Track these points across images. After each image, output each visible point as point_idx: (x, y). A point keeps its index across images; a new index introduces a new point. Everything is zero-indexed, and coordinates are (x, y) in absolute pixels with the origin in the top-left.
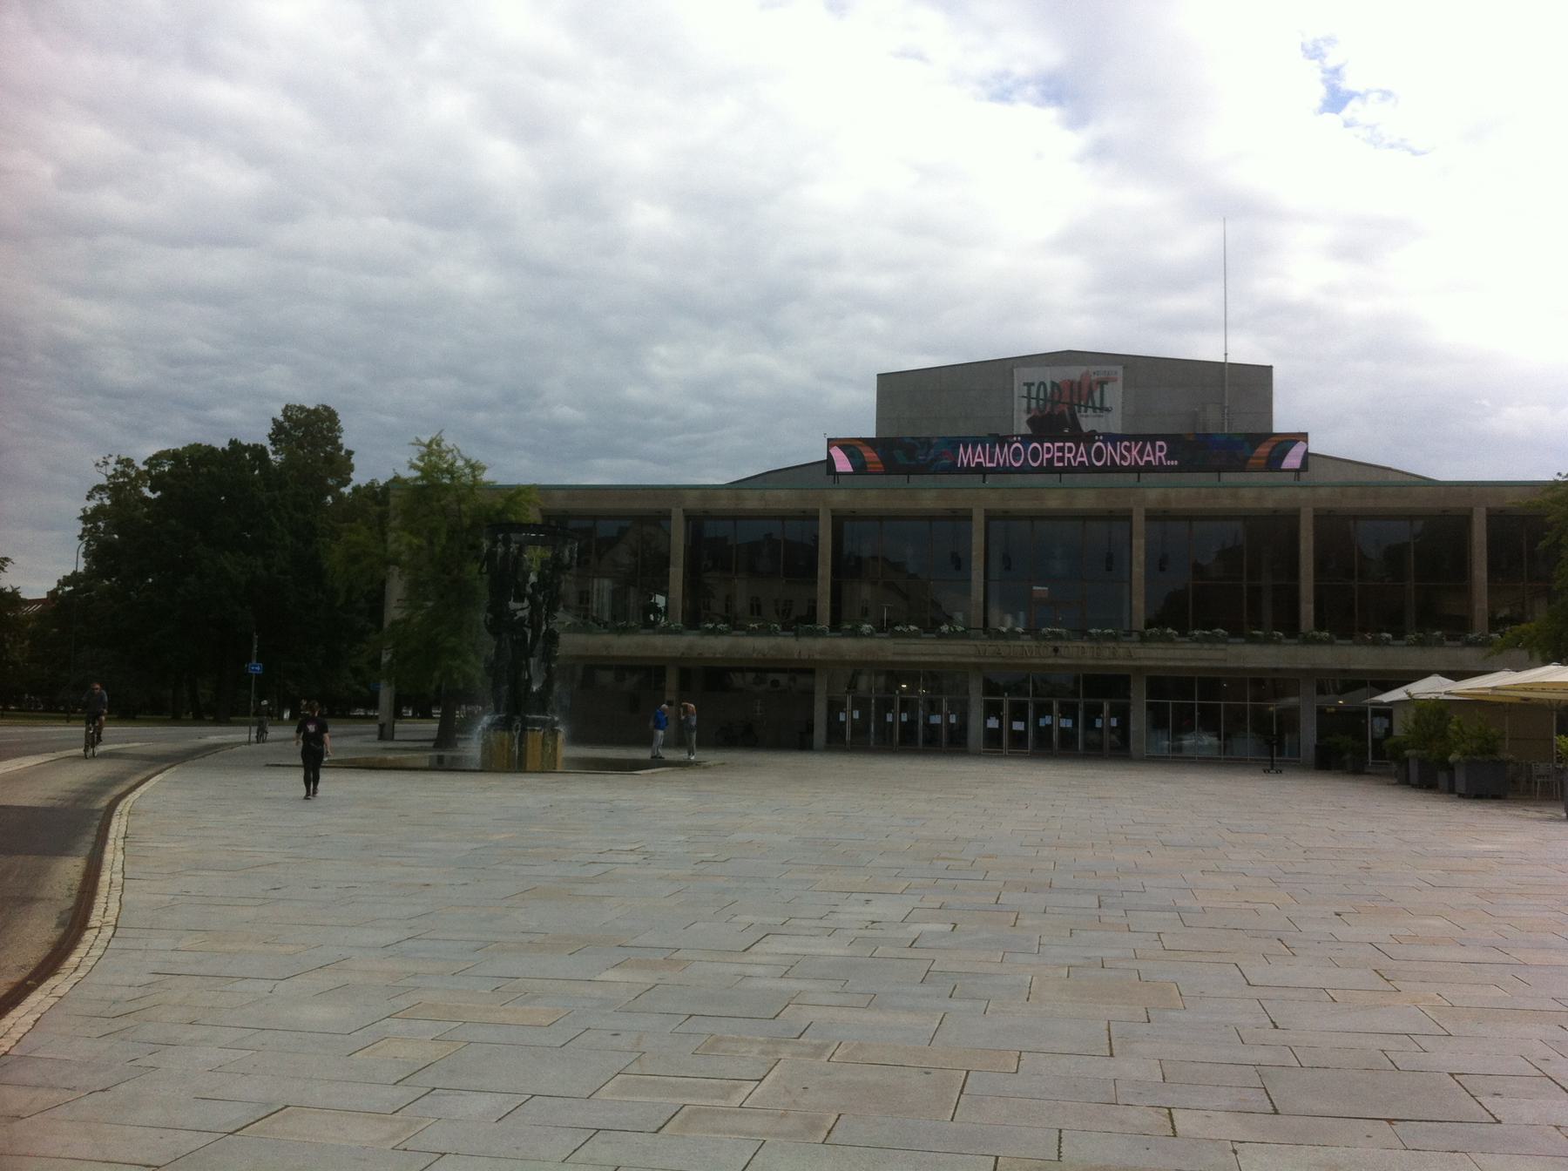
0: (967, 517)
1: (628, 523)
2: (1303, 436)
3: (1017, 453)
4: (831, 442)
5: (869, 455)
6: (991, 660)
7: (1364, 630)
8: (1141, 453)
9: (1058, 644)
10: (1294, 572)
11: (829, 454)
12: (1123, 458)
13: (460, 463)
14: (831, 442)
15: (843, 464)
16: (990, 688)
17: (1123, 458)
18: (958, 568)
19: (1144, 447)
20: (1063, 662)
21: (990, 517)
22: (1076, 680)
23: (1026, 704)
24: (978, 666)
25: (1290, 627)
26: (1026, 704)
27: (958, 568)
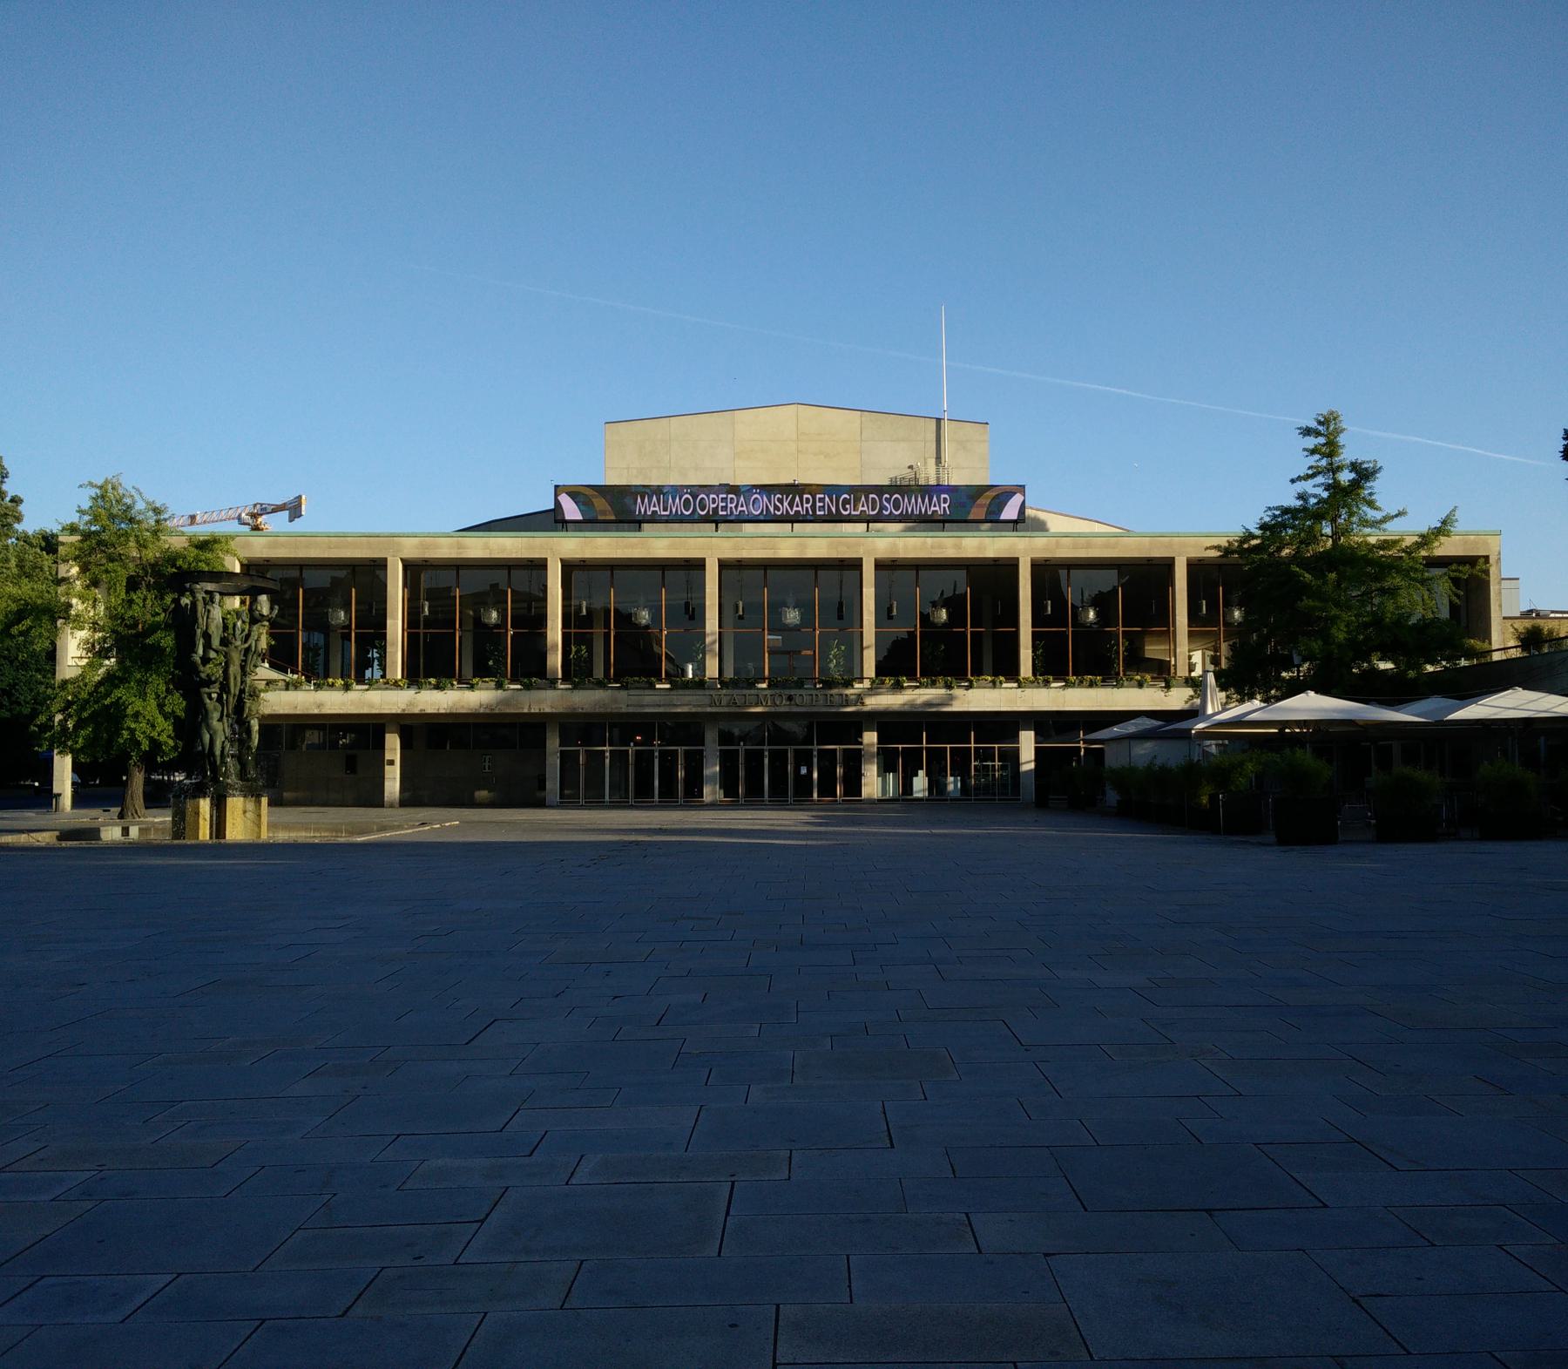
0: (856, 565)
1: (342, 574)
2: (1021, 489)
3: (687, 504)
4: (558, 489)
5: (600, 503)
6: (726, 710)
7: (427, 676)
8: (791, 505)
9: (792, 692)
10: (541, 620)
11: (557, 503)
12: (776, 508)
13: (140, 505)
14: (558, 489)
15: (571, 511)
16: (725, 738)
17: (776, 508)
18: (692, 618)
19: (793, 500)
20: (795, 709)
21: (724, 565)
22: (810, 727)
23: (819, 751)
24: (714, 717)
25: (1006, 669)
26: (819, 751)
27: (692, 618)
